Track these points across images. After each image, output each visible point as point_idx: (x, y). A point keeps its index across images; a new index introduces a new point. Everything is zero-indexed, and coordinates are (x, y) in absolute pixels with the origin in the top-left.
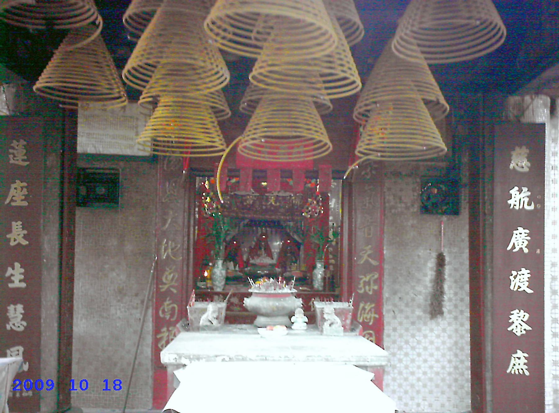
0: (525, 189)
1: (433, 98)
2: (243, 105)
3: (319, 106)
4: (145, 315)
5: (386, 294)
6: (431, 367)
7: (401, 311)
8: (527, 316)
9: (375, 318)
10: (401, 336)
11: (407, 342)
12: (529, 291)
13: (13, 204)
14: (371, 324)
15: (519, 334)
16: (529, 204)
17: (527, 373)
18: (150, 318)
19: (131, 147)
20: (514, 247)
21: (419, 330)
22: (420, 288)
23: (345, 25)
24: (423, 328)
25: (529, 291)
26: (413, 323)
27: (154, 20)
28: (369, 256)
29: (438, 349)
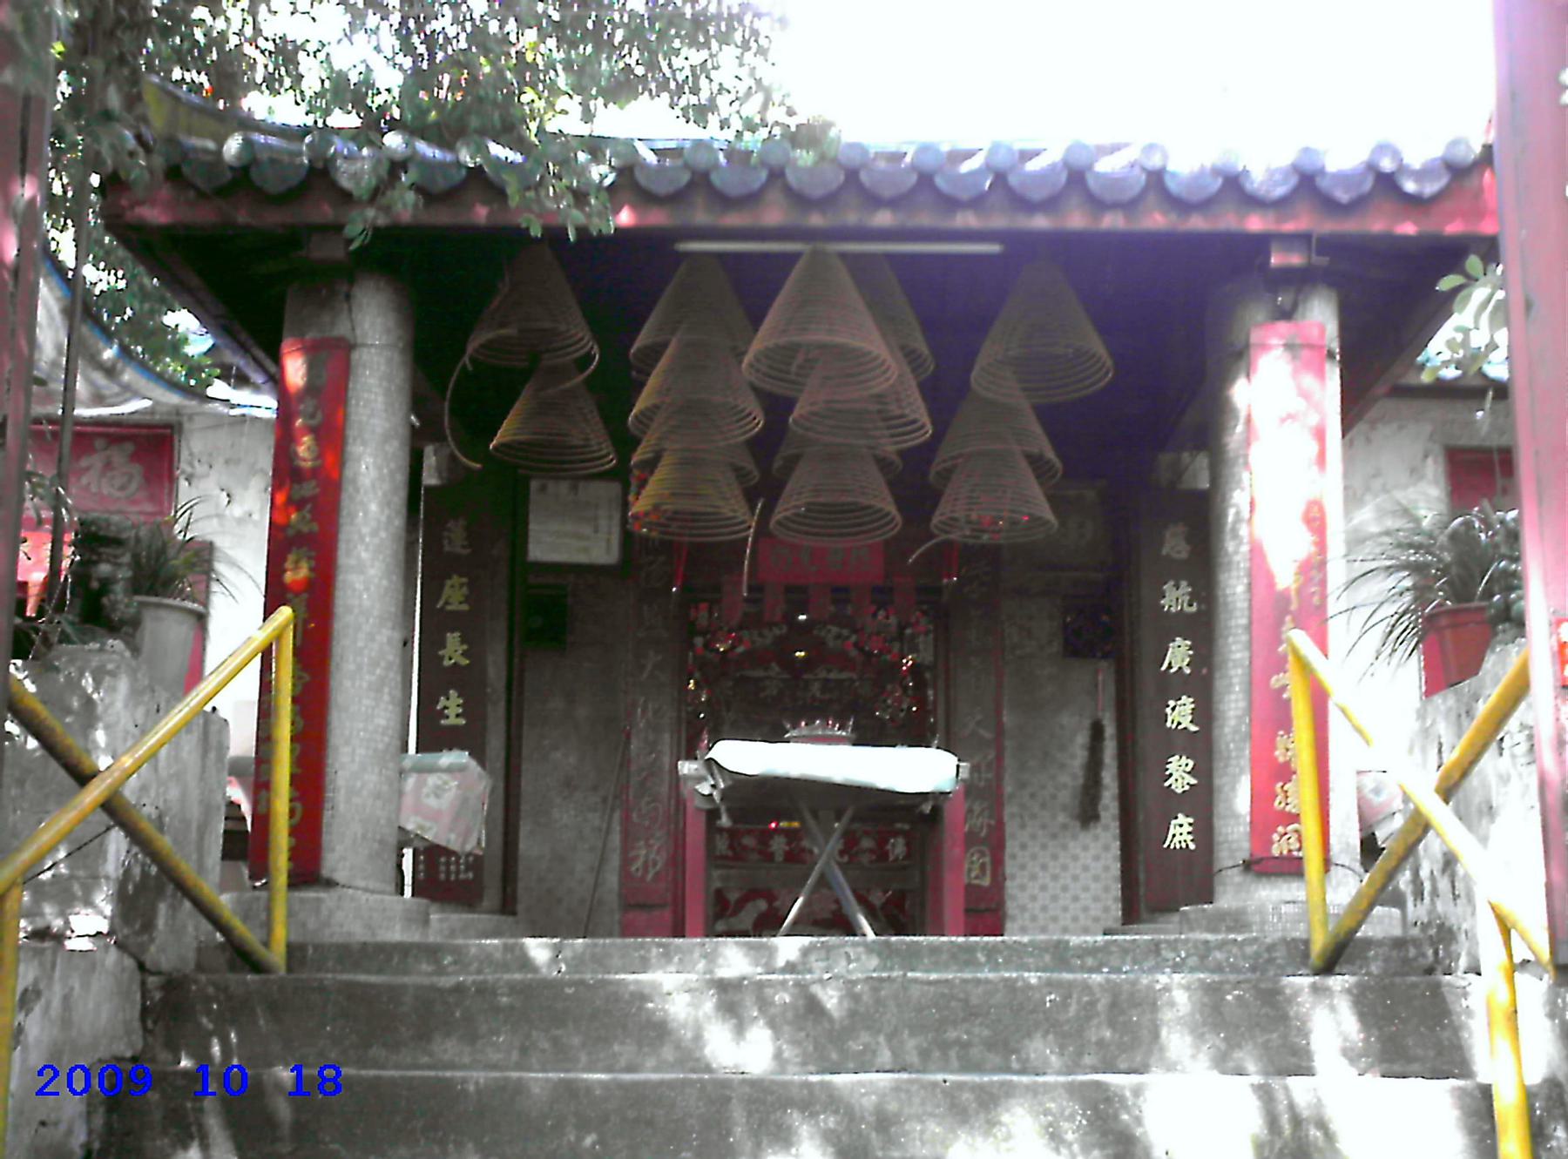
0: (1184, 584)
1: (1036, 451)
2: (778, 463)
3: (883, 464)
4: (611, 817)
5: (1008, 789)
6: (1086, 909)
7: (1034, 816)
8: (1191, 763)
9: (989, 826)
10: (1034, 857)
11: (1044, 867)
12: (1193, 728)
13: (449, 608)
14: (983, 834)
15: (1179, 791)
16: (1190, 605)
17: (1192, 846)
18: (617, 827)
19: (586, 550)
20: (1170, 666)
21: (1065, 847)
22: (1064, 778)
23: (911, 356)
24: (1071, 844)
25: (1193, 728)
26: (1054, 836)
27: (669, 351)
28: (979, 723)
29: (1096, 879)
